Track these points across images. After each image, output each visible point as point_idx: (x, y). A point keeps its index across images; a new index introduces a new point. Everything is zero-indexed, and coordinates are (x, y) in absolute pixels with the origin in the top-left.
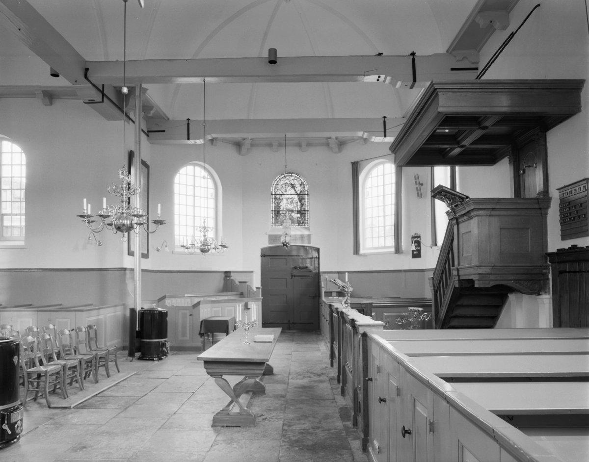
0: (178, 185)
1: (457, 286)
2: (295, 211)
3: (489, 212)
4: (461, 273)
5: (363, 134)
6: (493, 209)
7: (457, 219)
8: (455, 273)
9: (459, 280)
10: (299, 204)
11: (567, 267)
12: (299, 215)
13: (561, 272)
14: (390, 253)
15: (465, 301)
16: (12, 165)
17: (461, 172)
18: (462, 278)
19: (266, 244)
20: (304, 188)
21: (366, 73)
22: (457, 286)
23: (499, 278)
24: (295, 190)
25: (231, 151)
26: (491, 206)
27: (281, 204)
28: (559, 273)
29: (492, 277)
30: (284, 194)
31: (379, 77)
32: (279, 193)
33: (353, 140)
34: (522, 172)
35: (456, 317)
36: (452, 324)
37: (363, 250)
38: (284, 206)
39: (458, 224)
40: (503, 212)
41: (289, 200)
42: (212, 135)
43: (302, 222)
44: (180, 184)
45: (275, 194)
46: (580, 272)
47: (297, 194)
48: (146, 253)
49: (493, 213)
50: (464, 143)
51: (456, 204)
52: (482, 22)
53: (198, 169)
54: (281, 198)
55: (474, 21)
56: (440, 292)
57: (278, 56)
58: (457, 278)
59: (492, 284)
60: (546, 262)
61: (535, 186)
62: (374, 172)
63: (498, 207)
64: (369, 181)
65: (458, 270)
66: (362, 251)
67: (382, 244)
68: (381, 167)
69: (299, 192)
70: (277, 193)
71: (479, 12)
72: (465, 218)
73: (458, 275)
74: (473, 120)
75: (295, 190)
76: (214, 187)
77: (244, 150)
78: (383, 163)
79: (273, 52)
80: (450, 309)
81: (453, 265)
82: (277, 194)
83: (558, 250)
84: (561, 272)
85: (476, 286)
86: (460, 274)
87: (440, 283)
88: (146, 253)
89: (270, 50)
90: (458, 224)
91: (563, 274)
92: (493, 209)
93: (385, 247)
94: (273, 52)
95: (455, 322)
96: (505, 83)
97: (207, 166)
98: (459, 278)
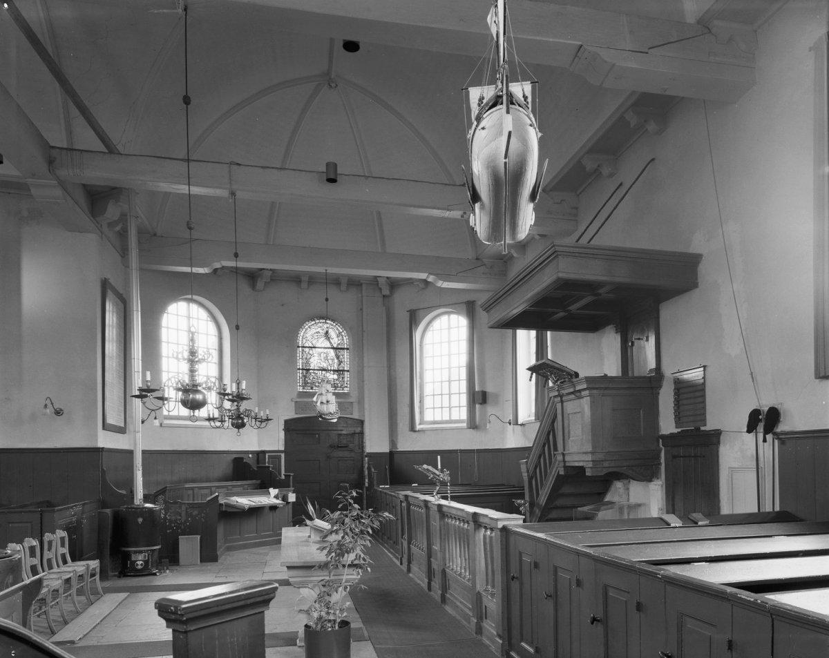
0: (166, 329)
1: (562, 473)
2: (331, 370)
3: (602, 392)
4: (567, 458)
5: (428, 277)
6: (606, 389)
7: (561, 396)
8: (560, 458)
9: (565, 467)
10: (336, 361)
11: (681, 451)
12: (335, 377)
13: (674, 457)
14: (462, 429)
15: (566, 489)
16: (434, 408)
17: (551, 335)
18: (567, 464)
19: (291, 415)
20: (343, 340)
21: (450, 208)
22: (562, 473)
23: (613, 464)
24: (330, 343)
25: (244, 287)
26: (599, 384)
27: (311, 360)
28: (672, 458)
29: (606, 464)
30: (315, 347)
31: (465, 213)
32: (307, 345)
33: (410, 282)
34: (630, 344)
35: (557, 508)
36: (550, 516)
37: (420, 424)
38: (315, 362)
39: (562, 402)
40: (614, 392)
41: (322, 355)
42: (222, 262)
43: (339, 385)
44: (168, 328)
45: (304, 347)
46: (695, 456)
47: (333, 348)
48: (122, 425)
49: (606, 392)
50: (570, 308)
51: (563, 380)
52: (589, 165)
53: (194, 307)
54: (311, 352)
55: (579, 162)
56: (536, 478)
57: (339, 171)
58: (562, 464)
59: (605, 471)
60: (658, 445)
61: (645, 360)
62: (437, 324)
63: (611, 386)
64: (429, 335)
65: (563, 455)
66: (418, 427)
67: (446, 418)
68: (445, 318)
69: (335, 346)
70: (305, 345)
71: (587, 153)
72: (573, 396)
73: (564, 461)
74: (590, 287)
75: (330, 343)
76: (217, 335)
77: (260, 284)
78: (448, 313)
79: (332, 166)
80: (551, 498)
81: (556, 449)
82: (306, 347)
83: (671, 434)
84: (674, 457)
85: (587, 474)
86: (566, 460)
87: (536, 468)
88: (122, 425)
89: (328, 165)
90: (562, 402)
91: (677, 459)
92: (606, 389)
93: (451, 422)
94: (332, 166)
95: (554, 514)
96: (629, 252)
97: (195, 297)
98: (565, 464)
